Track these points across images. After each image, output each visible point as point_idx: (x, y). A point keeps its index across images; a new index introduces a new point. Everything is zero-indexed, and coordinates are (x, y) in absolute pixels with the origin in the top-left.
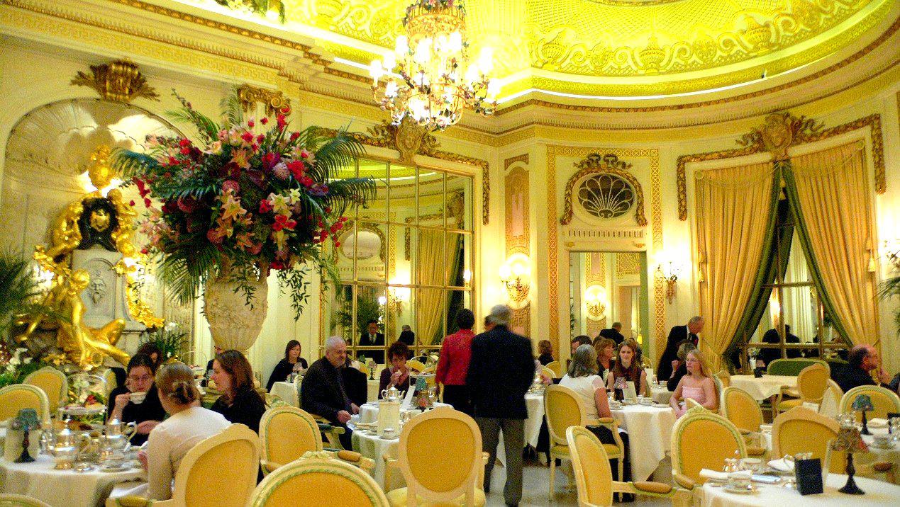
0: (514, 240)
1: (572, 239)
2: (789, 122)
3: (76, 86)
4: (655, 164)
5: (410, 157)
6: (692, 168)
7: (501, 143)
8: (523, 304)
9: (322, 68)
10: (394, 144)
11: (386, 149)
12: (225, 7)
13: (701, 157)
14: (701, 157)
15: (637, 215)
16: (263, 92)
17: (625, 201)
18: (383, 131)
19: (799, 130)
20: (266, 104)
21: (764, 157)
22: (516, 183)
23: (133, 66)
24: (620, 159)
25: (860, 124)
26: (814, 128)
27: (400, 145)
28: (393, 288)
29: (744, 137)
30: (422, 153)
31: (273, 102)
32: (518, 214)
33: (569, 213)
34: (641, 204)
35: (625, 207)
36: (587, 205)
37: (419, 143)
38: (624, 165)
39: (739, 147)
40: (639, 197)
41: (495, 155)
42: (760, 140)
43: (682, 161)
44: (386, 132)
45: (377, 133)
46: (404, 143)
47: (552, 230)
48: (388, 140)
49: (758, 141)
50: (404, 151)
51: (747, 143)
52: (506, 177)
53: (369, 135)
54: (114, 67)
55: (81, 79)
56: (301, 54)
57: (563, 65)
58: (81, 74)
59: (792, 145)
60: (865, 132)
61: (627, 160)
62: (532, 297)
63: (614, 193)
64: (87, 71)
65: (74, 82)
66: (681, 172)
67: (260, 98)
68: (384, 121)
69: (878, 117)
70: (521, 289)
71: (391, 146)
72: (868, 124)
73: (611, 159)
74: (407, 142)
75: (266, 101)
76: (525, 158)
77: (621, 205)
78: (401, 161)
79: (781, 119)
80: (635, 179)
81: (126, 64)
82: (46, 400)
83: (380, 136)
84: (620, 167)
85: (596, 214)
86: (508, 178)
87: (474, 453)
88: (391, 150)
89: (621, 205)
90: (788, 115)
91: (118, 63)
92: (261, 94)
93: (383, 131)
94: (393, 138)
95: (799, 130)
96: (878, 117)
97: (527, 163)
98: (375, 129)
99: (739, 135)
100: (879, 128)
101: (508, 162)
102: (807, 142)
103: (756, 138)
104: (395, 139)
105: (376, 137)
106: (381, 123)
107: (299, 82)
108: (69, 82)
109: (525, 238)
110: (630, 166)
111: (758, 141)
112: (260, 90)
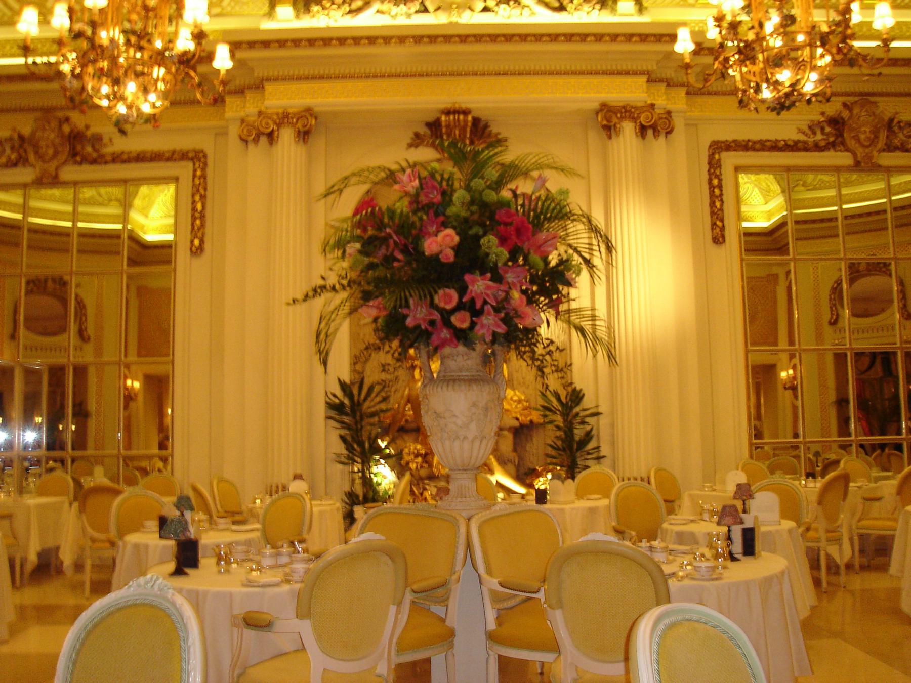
3: (413, 149)
5: (871, 158)
10: (843, 143)
11: (831, 153)
12: (564, 13)
16: (628, 108)
18: (823, 129)
20: (636, 122)
23: (466, 112)
27: (851, 143)
28: (71, 196)
30: (890, 148)
31: (643, 119)
37: (883, 135)
44: (828, 129)
45: (814, 133)
46: (858, 140)
48: (831, 139)
50: (860, 151)
53: (802, 137)
54: (443, 118)
55: (417, 140)
58: (417, 135)
64: (423, 130)
65: (410, 146)
67: (625, 117)
68: (823, 114)
71: (838, 148)
74: (862, 137)
75: (634, 119)
79: (54, 124)
81: (456, 112)
82: (743, 637)
83: (819, 136)
88: (839, 153)
90: (67, 120)
91: (448, 112)
92: (626, 112)
93: (823, 129)
94: (840, 134)
98: (810, 127)
104: (841, 135)
105: (811, 140)
107: (682, 85)
108: (406, 146)
112: (624, 107)
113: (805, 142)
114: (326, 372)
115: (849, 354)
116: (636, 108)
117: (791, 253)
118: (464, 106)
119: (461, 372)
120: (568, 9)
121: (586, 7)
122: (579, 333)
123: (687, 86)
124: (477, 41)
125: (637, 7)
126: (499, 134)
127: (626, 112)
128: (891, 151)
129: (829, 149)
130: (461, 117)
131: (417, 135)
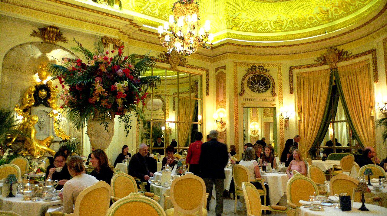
0: (219, 103)
1: (244, 102)
2: (337, 52)
3: (33, 37)
4: (280, 70)
5: (175, 67)
6: (295, 71)
7: (214, 61)
8: (223, 130)
9: (137, 29)
10: (168, 61)
13: (300, 67)
14: (300, 67)
15: (272, 92)
17: (267, 86)
18: (164, 56)
19: (341, 55)
20: (114, 44)
21: (326, 67)
22: (220, 78)
24: (265, 68)
25: (367, 53)
26: (348, 54)
27: (171, 62)
29: (318, 58)
31: (116, 44)
32: (221, 91)
33: (243, 91)
34: (274, 87)
35: (267, 88)
36: (251, 88)
38: (266, 70)
39: (316, 63)
40: (273, 84)
41: (211, 67)
42: (325, 60)
43: (291, 69)
44: (165, 56)
45: (161, 57)
46: (172, 61)
47: (236, 98)
48: (166, 60)
49: (324, 60)
50: (173, 64)
51: (319, 61)
52: (216, 76)
53: (157, 57)
55: (34, 34)
56: (128, 23)
57: (240, 28)
58: (34, 32)
59: (338, 62)
60: (369, 56)
61: (268, 68)
62: (227, 126)
63: (262, 82)
65: (31, 35)
66: (291, 73)
68: (164, 52)
69: (375, 50)
70: (222, 123)
72: (371, 53)
73: (261, 68)
74: (174, 60)
75: (114, 43)
76: (224, 67)
77: (265, 88)
78: (171, 69)
80: (271, 76)
83: (162, 58)
84: (265, 71)
85: (254, 92)
86: (217, 76)
87: (202, 193)
89: (265, 88)
91: (51, 27)
92: (111, 40)
93: (164, 56)
94: (168, 59)
95: (341, 55)
96: (375, 50)
97: (225, 70)
98: (160, 55)
99: (315, 58)
100: (375, 55)
101: (217, 69)
102: (345, 61)
103: (323, 59)
105: (160, 58)
106: (162, 53)
108: (30, 35)
109: (224, 102)
110: (269, 71)
111: (324, 60)
112: (111, 38)
113: (159, 59)
114: (127, 136)
115: (332, 147)
116: (115, 39)
117: (336, 147)
118: (57, 26)
119: (149, 136)
120: (98, 2)
121: (104, 3)
122: (199, 130)
123: (119, 30)
124: (66, 5)
125: (120, 8)
126: (66, 38)
127: (111, 40)
128: (180, 66)
129: (164, 63)
130: (55, 30)
131: (34, 32)
